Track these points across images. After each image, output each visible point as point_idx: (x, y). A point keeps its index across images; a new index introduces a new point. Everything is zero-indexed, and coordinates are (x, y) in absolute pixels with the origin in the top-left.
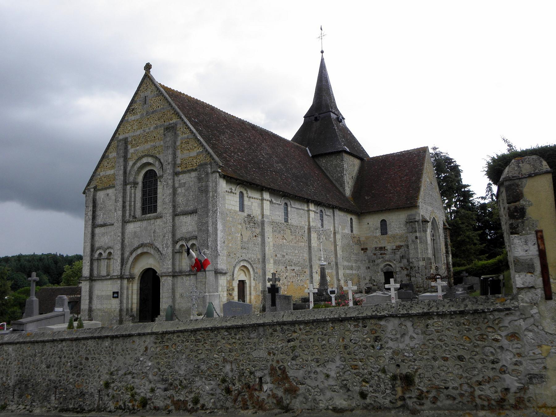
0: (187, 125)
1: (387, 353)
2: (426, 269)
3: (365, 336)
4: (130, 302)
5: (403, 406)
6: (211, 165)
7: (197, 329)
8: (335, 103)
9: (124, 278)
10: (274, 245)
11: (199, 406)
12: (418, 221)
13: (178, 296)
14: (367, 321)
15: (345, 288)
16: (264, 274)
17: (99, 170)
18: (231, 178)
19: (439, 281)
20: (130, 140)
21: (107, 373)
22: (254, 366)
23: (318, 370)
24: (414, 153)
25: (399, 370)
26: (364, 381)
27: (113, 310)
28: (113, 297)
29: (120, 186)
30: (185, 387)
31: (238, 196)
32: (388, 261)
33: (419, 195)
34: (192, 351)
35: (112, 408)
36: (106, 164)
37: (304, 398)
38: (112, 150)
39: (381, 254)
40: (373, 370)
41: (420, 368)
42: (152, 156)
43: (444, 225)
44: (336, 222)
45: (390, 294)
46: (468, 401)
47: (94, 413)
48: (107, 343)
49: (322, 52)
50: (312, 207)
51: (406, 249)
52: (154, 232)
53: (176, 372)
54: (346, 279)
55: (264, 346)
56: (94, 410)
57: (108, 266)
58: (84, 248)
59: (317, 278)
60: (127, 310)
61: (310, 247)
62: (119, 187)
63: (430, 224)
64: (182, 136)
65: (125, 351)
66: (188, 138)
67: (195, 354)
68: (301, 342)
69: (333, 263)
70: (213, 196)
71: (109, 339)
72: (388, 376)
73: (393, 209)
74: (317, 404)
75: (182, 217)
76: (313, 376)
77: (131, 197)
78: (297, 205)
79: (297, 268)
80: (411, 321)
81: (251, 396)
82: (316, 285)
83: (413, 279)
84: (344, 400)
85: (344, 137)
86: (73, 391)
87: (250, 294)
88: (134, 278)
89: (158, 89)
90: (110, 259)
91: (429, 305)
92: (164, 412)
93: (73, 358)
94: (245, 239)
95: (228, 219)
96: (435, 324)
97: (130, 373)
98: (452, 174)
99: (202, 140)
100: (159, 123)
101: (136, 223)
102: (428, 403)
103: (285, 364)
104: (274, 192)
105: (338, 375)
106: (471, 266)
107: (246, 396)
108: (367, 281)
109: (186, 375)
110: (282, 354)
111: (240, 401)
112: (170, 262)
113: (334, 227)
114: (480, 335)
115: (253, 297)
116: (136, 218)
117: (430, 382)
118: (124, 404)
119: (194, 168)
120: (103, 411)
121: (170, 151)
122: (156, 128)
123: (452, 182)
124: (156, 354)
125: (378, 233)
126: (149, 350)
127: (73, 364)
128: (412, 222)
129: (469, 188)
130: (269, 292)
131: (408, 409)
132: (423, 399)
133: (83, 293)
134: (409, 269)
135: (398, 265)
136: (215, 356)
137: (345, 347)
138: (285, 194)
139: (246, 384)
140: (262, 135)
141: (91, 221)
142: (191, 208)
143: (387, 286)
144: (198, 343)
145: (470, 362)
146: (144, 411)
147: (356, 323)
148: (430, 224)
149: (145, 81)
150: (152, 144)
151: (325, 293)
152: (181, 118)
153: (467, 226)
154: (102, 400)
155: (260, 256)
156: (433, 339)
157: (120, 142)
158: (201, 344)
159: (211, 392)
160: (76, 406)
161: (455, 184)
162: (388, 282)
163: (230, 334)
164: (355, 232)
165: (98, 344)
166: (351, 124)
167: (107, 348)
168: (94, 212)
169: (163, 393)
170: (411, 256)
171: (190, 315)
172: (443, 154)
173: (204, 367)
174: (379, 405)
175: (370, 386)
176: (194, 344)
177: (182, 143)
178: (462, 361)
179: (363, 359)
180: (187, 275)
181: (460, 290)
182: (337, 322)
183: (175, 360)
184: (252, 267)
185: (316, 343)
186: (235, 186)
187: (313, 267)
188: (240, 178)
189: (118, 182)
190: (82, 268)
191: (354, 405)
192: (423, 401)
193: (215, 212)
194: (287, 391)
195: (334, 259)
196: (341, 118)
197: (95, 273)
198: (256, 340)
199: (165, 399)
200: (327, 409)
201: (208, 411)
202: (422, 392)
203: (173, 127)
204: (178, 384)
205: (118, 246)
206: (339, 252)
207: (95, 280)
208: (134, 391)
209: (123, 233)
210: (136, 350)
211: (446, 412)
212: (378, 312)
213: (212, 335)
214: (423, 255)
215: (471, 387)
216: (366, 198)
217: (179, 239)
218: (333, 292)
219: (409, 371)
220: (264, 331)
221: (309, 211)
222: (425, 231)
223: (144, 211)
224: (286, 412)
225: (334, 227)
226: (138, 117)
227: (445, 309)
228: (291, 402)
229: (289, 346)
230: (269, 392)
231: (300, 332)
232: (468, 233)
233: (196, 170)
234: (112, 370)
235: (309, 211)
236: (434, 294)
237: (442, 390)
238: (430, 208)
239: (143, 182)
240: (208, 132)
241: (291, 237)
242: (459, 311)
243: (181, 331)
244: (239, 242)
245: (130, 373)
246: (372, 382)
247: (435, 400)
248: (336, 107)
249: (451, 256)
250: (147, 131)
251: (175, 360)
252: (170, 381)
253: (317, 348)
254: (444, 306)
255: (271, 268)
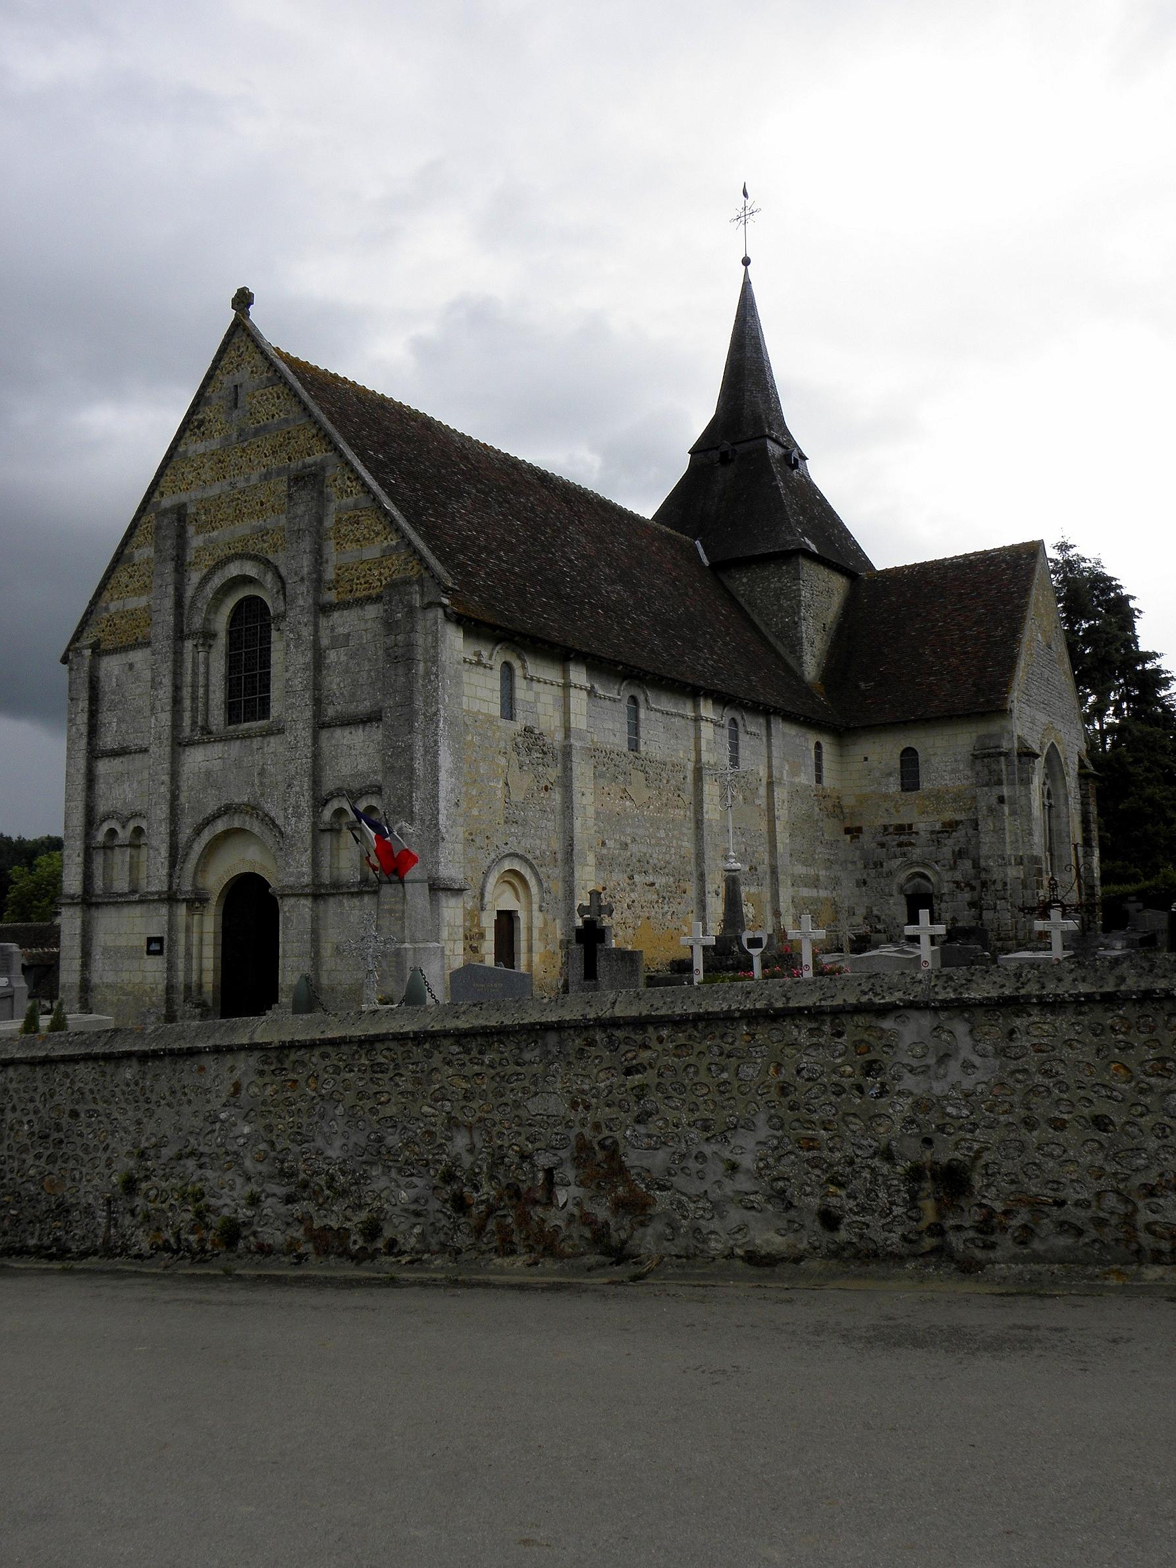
0: (353, 470)
1: (898, 1108)
2: (1025, 887)
3: (839, 1061)
4: (195, 967)
5: (936, 1251)
6: (422, 586)
7: (377, 1036)
8: (779, 411)
9: (178, 901)
10: (597, 813)
11: (380, 1244)
12: (1006, 755)
13: (327, 950)
14: (844, 1019)
15: (792, 933)
16: (570, 893)
17: (106, 595)
18: (479, 623)
19: (1055, 914)
20: (191, 510)
21: (130, 1154)
22: (532, 1139)
23: (708, 1149)
24: (1004, 561)
25: (928, 1153)
26: (833, 1181)
27: (147, 987)
28: (149, 952)
29: (165, 643)
30: (344, 1193)
31: (497, 674)
32: (918, 864)
33: (1011, 679)
34: (361, 1095)
35: (145, 1246)
36: (124, 579)
37: (669, 1225)
38: (142, 539)
39: (900, 845)
40: (859, 1152)
41: (988, 1149)
42: (254, 558)
43: (1082, 765)
44: (775, 754)
45: (918, 952)
46: (1117, 1240)
47: (94, 1259)
48: (128, 1073)
49: (746, 262)
50: (707, 710)
51: (971, 832)
52: (262, 773)
53: (319, 1152)
54: (797, 915)
55: (559, 1085)
56: (95, 1253)
57: (133, 867)
58: (67, 816)
59: (716, 907)
60: (188, 987)
61: (699, 823)
62: (164, 645)
63: (1040, 763)
64: (341, 500)
65: (179, 1094)
66: (356, 507)
67: (370, 1104)
68: (660, 1075)
69: (764, 868)
70: (428, 673)
71: (134, 1063)
72: (899, 1169)
73: (937, 718)
74: (705, 1241)
75: (338, 732)
76: (693, 1165)
77: (195, 673)
78: (666, 703)
79: (661, 881)
80: (967, 1020)
81: (524, 1220)
82: (715, 929)
83: (988, 915)
84: (778, 1231)
85: (803, 511)
86: (39, 1202)
87: (530, 949)
88: (207, 900)
89: (271, 364)
90: (139, 847)
91: (1018, 976)
92: (286, 1259)
93: (36, 1112)
94: (518, 797)
95: (469, 738)
96: (1034, 1028)
97: (192, 1154)
98: (1110, 624)
99: (395, 513)
100: (274, 463)
101: (209, 747)
102: (1006, 1244)
103: (618, 1135)
104: (599, 666)
105: (761, 1165)
106: (1153, 883)
107: (510, 1220)
108: (859, 919)
109: (344, 1161)
110: (608, 1106)
111: (493, 1233)
112: (306, 858)
113: (770, 767)
114: (1157, 1059)
115: (536, 958)
116: (210, 733)
117: (1013, 1188)
118: (177, 1236)
119: (373, 592)
120: (120, 1255)
121: (306, 544)
122: (266, 477)
123: (1109, 642)
124: (264, 1103)
125: (893, 786)
126: (243, 1092)
127: (36, 1128)
128: (989, 755)
129: (1158, 661)
130: (578, 941)
131: (951, 1258)
132: (992, 1232)
133: (65, 941)
134: (978, 888)
135: (947, 876)
136: (426, 1109)
137: (784, 1090)
138: (634, 671)
139: (508, 1186)
140: (568, 502)
141: (84, 741)
142: (365, 706)
143: (910, 930)
144: (379, 1076)
145: (1128, 1134)
146: (232, 1255)
147: (814, 1025)
148: (1040, 763)
149: (236, 340)
150: (254, 522)
151: (736, 949)
152: (336, 449)
153: (1148, 770)
154: (115, 1226)
155: (557, 845)
156: (1025, 1071)
157: (163, 515)
158: (386, 1076)
159: (413, 1207)
160: (46, 1241)
161: (1118, 650)
162: (914, 919)
163: (467, 1051)
164: (826, 781)
165: (104, 1074)
166: (829, 474)
167: (128, 1085)
168: (93, 714)
169: (282, 1209)
170: (985, 850)
171: (360, 1002)
172: (1088, 565)
173: (393, 1140)
174: (872, 1246)
175: (849, 1196)
176: (367, 1076)
177: (339, 521)
178: (1105, 1131)
179: (830, 1122)
180: (352, 894)
181: (1119, 945)
182: (761, 1020)
183: (316, 1119)
184: (536, 874)
185: (703, 1077)
186: (490, 647)
187: (708, 878)
188: (504, 624)
189: (159, 630)
190: (60, 875)
191: (803, 1245)
192: (993, 1239)
193: (432, 718)
194: (622, 1206)
195: (766, 857)
196: (795, 455)
197: (98, 884)
198: (538, 1068)
199: (288, 1224)
200: (731, 1255)
201: (405, 1259)
202: (991, 1213)
203: (315, 475)
204: (323, 1183)
205: (161, 812)
206: (783, 838)
207: (98, 905)
208: (202, 1203)
209: (174, 775)
210: (208, 1091)
211: (1056, 1267)
212: (876, 994)
213: (418, 1053)
214: (1017, 849)
215: (1127, 1201)
216: (863, 685)
217: (331, 793)
218: (755, 943)
219: (958, 1155)
220: (561, 1043)
221: (697, 719)
222: (1026, 782)
223: (234, 713)
224: (618, 1264)
225: (770, 767)
226: (214, 444)
227: (1064, 989)
228: (630, 1237)
229: (629, 1085)
230: (571, 1208)
231: (659, 1047)
232: (1149, 791)
233: (378, 599)
234: (144, 1144)
235: (697, 719)
236: (1041, 955)
237: (1046, 1209)
238: (1042, 718)
239: (230, 633)
240: (414, 490)
241: (647, 793)
242: (1103, 995)
243: (332, 1042)
244: (500, 805)
245: (192, 1154)
246: (856, 1184)
247: (1026, 1235)
248: (782, 425)
249: (1097, 852)
250: (241, 485)
251: (316, 1119)
252: (302, 1176)
253: (705, 1091)
254: (1060, 980)
255: (587, 878)
